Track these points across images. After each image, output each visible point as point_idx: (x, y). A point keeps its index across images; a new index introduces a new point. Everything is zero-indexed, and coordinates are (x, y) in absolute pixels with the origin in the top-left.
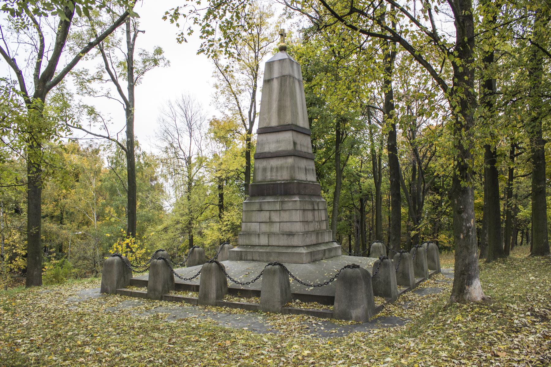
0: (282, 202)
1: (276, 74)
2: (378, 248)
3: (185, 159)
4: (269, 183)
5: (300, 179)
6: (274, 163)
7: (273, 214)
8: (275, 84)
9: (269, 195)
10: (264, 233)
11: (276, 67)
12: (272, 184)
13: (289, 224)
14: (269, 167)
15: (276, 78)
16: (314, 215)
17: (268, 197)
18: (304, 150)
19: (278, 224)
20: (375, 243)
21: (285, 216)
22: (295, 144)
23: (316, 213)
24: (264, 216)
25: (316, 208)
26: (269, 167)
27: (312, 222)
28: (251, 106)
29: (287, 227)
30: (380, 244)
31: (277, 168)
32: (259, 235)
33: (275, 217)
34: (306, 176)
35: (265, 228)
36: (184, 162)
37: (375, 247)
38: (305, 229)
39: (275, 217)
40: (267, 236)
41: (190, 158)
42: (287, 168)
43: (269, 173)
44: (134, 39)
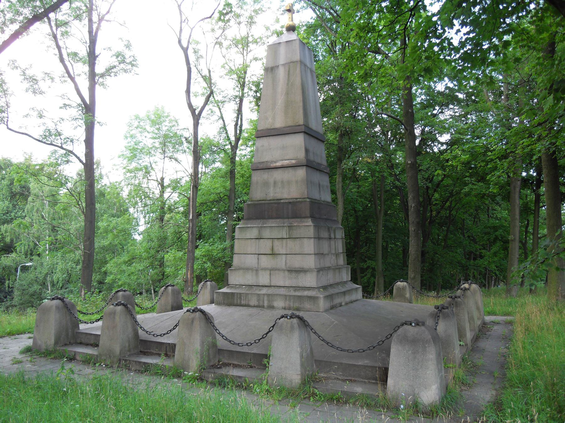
0: (290, 227)
1: (282, 60)
2: (404, 288)
3: (157, 181)
4: (272, 202)
5: (314, 198)
6: (278, 175)
7: (276, 243)
8: (281, 73)
9: (271, 218)
10: (265, 269)
11: (282, 51)
12: (275, 203)
13: (299, 257)
14: (271, 181)
15: (283, 65)
16: (330, 246)
17: (271, 221)
18: (318, 160)
19: (284, 256)
20: (399, 283)
21: (293, 245)
22: (307, 151)
23: (332, 242)
24: (265, 246)
25: (333, 236)
26: (271, 181)
27: (328, 254)
28: (238, 118)
29: (297, 262)
30: (405, 283)
31: (282, 182)
32: (257, 270)
33: (280, 247)
34: (320, 195)
35: (265, 262)
36: (156, 184)
37: (399, 289)
38: (320, 264)
39: (280, 247)
40: (268, 272)
41: (162, 179)
42: (297, 182)
43: (272, 188)
44: (98, 29)
